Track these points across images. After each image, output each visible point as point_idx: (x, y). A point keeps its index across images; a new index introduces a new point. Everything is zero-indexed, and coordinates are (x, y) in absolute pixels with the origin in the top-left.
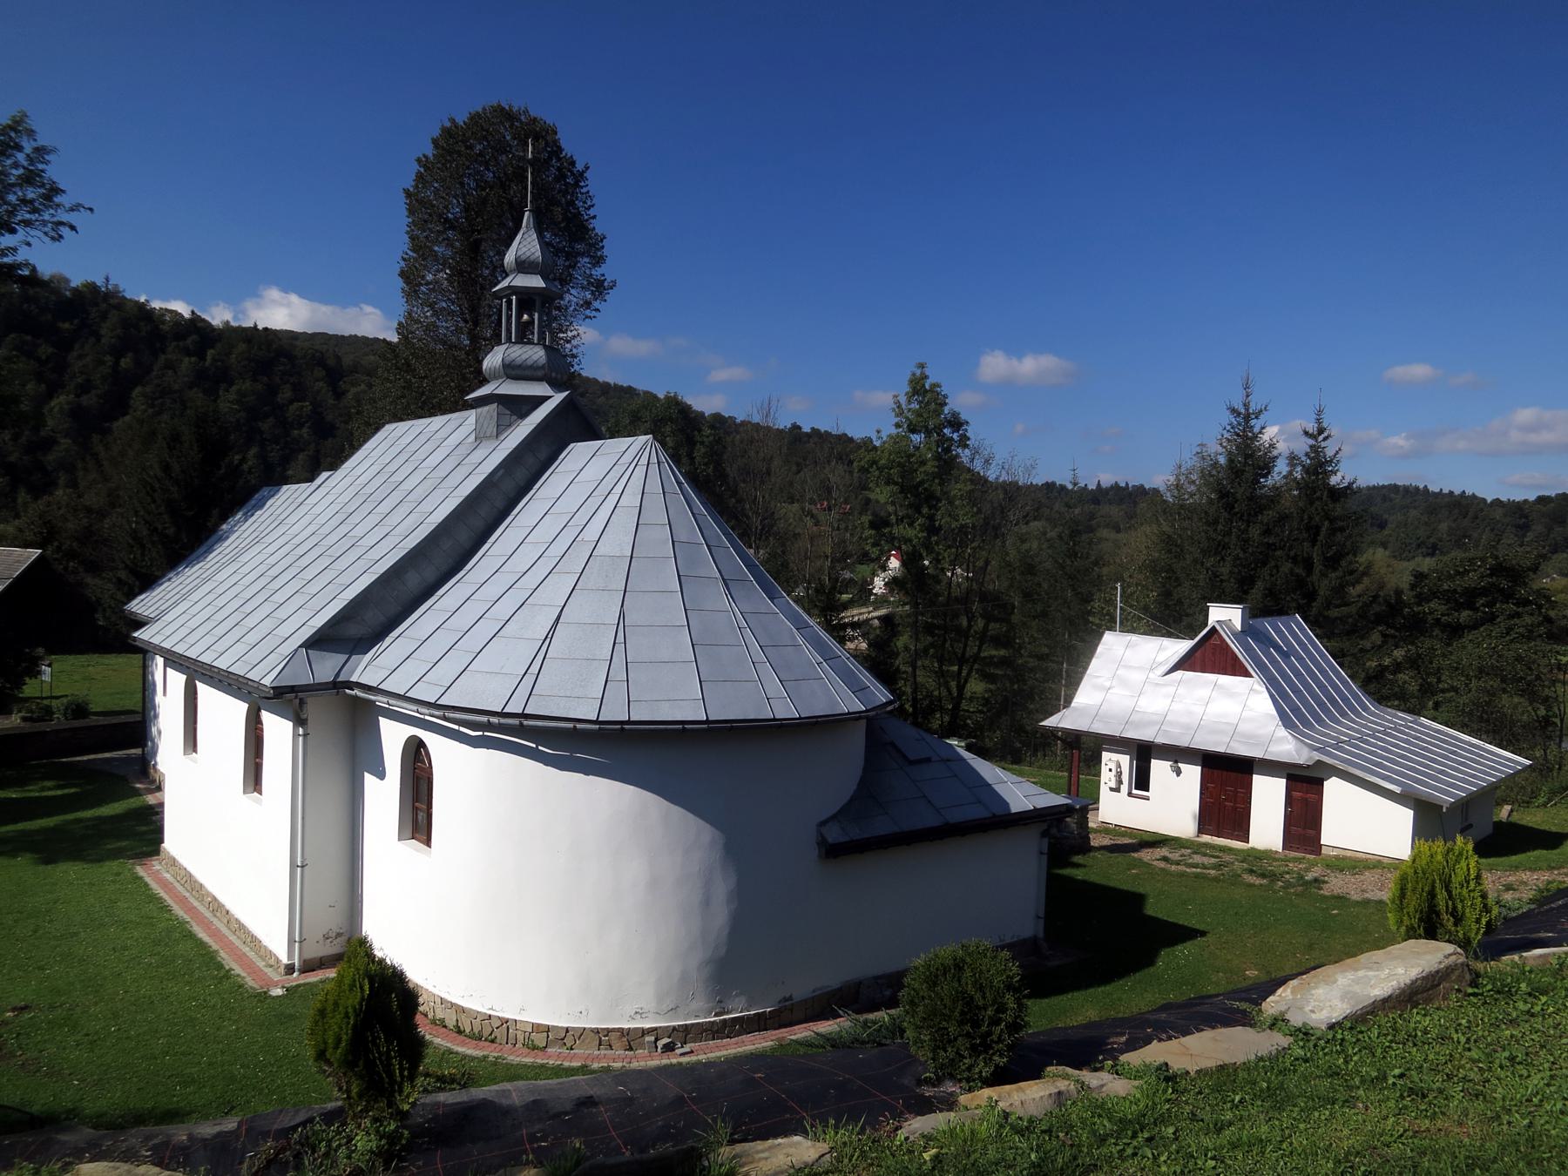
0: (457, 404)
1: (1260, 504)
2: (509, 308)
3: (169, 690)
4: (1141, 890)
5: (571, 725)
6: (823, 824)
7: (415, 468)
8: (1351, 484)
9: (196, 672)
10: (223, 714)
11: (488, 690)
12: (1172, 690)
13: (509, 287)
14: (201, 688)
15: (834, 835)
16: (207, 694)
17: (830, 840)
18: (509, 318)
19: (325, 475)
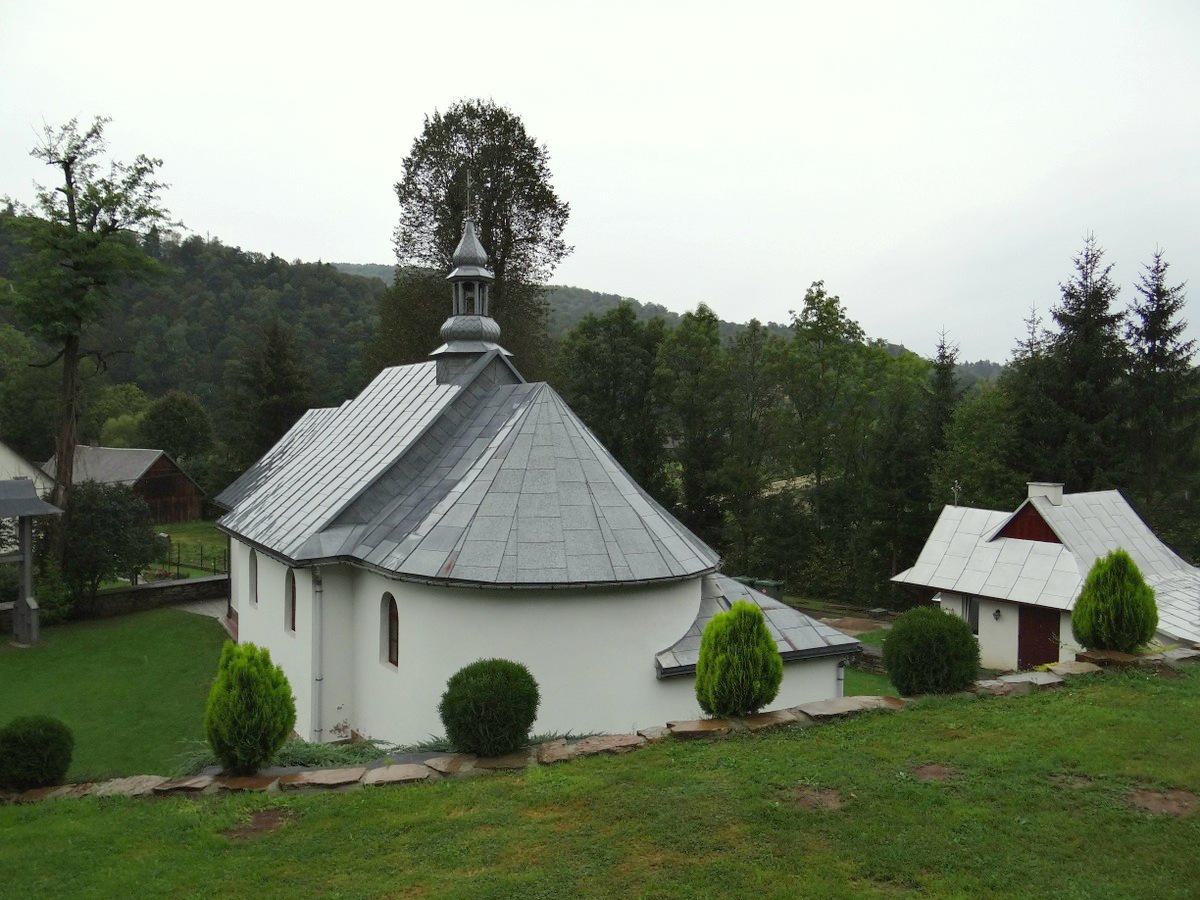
0: (422, 356)
1: (529, 297)
2: (457, 289)
3: (239, 555)
4: (1066, 496)
5: (538, 587)
6: (660, 654)
7: (405, 398)
8: (437, 117)
9: (255, 547)
10: (272, 578)
11: (427, 563)
12: (1058, 523)
13: (455, 276)
14: (258, 554)
15: (668, 662)
16: (263, 561)
17: (664, 666)
18: (457, 296)
19: (348, 402)
